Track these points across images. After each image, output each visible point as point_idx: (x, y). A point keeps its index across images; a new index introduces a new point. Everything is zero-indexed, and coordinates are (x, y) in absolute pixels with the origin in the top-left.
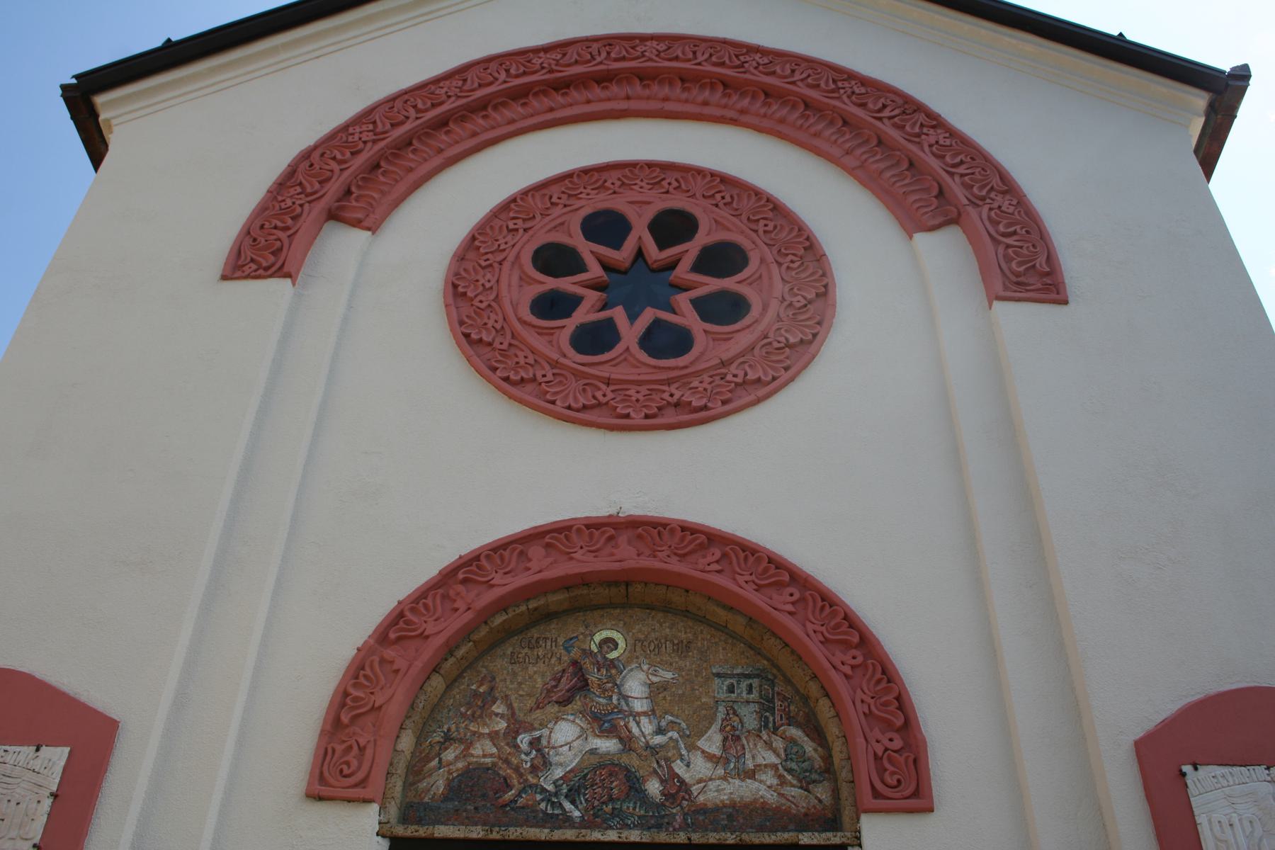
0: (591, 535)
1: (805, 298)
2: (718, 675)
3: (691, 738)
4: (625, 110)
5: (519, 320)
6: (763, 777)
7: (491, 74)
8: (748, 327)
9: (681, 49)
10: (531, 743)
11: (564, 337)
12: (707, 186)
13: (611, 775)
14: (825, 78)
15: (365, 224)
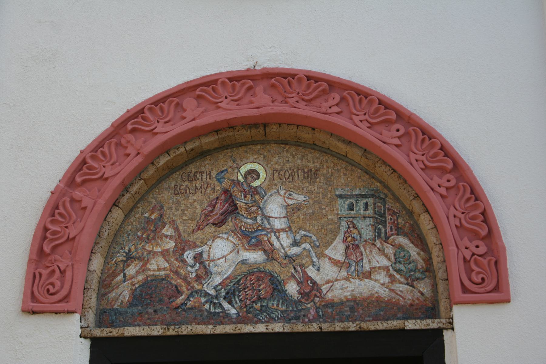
0: (234, 87)
2: (340, 196)
6: (378, 277)
10: (195, 258)
13: (258, 280)
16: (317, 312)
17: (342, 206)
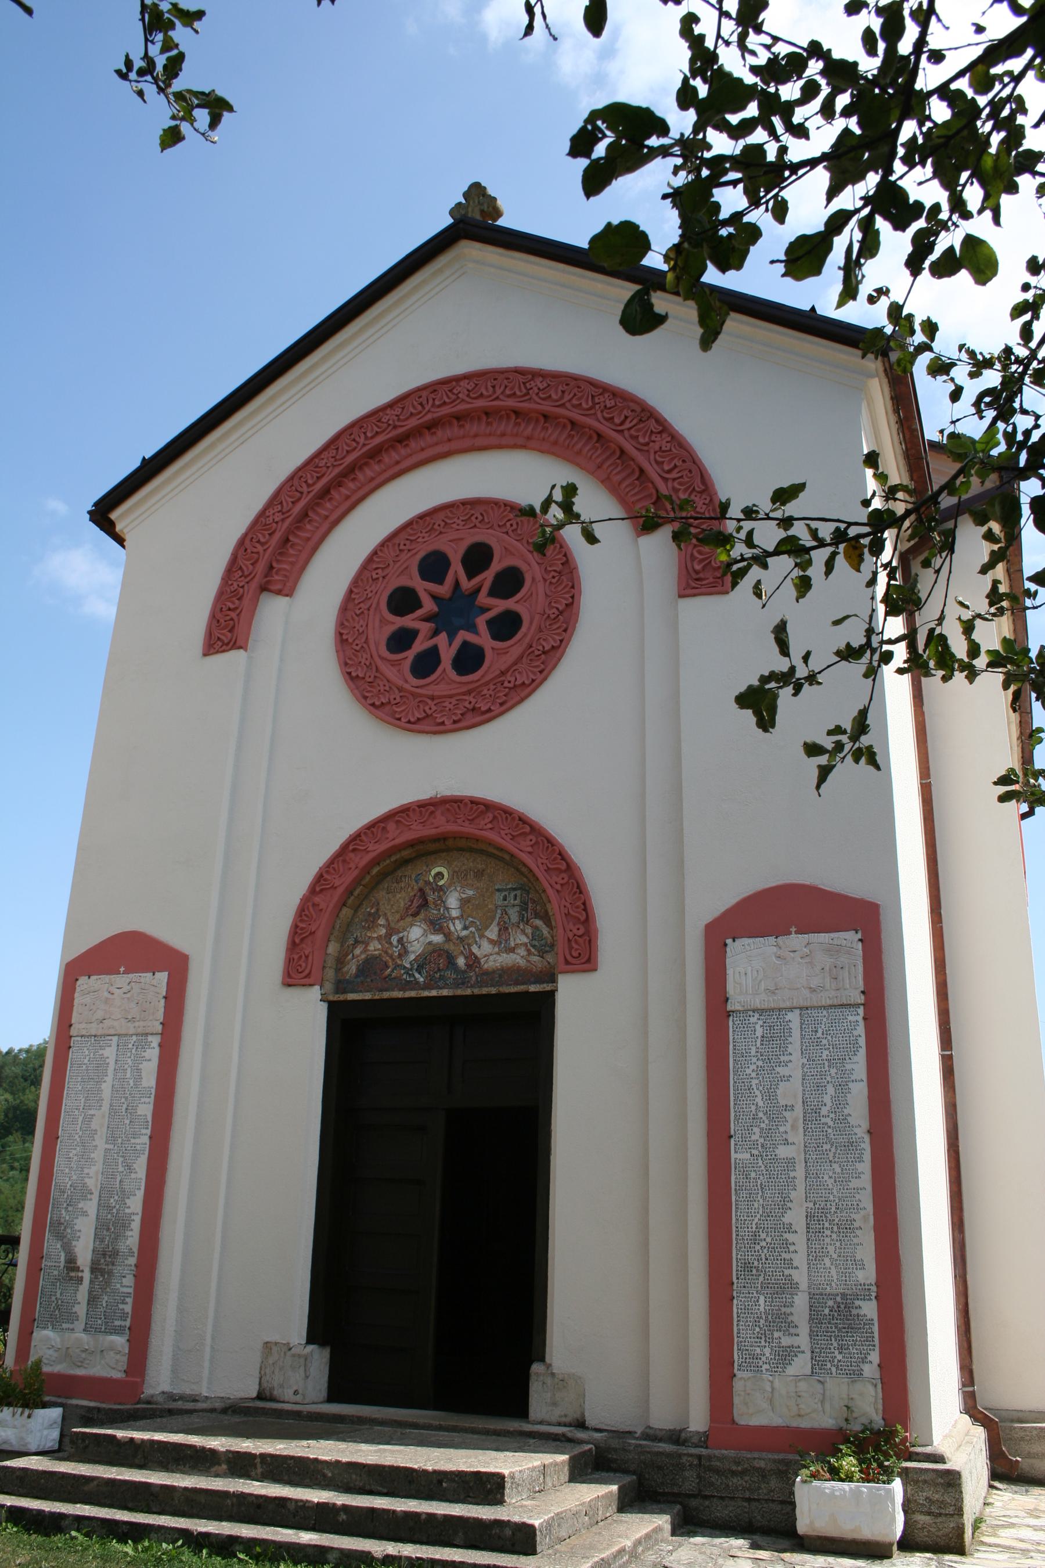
2: (498, 890)
3: (481, 932)
5: (380, 656)
6: (519, 951)
8: (519, 641)
13: (439, 956)
14: (585, 397)
15: (284, 592)
16: (477, 979)
17: (498, 898)
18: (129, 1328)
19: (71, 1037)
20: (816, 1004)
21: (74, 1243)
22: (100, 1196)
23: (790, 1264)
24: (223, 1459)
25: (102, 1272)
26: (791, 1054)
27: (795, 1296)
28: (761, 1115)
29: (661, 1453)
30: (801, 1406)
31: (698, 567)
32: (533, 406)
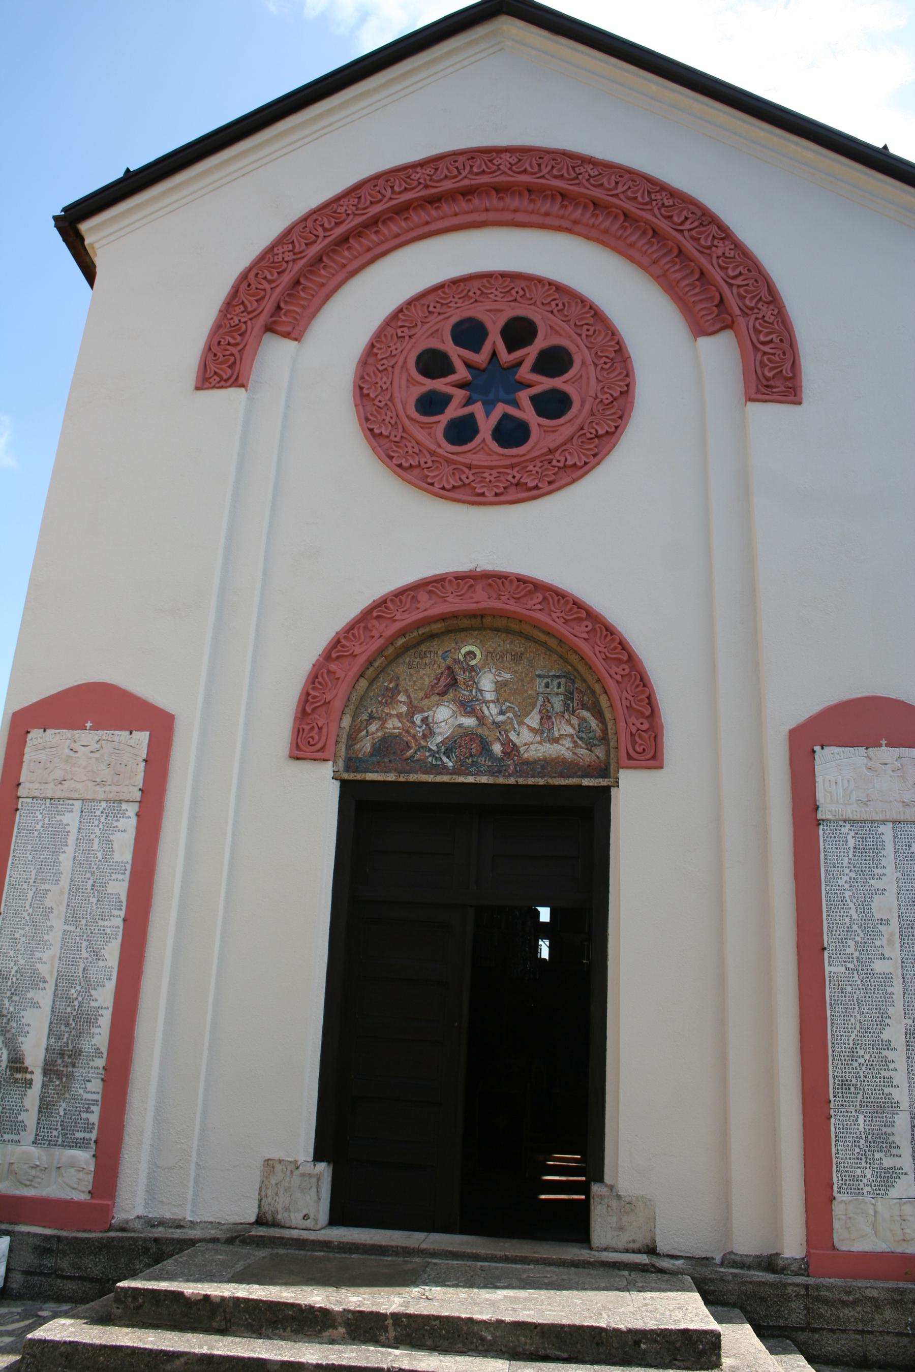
0: (458, 584)
1: (612, 395)
2: (539, 676)
4: (485, 222)
5: (408, 416)
6: (564, 742)
7: (379, 192)
8: (570, 421)
9: (528, 161)
10: (422, 720)
11: (440, 430)
12: (545, 295)
13: (471, 741)
14: (641, 191)
15: (293, 335)
16: (515, 768)
17: (540, 684)
18: (96, 1142)
19: (19, 798)
20: (909, 819)
21: (20, 1039)
22: (56, 986)
23: (889, 1082)
24: (339, 1320)
25: (60, 1076)
26: (884, 867)
27: (895, 1116)
28: (855, 927)
29: (763, 1283)
30: (905, 1231)
31: (770, 375)
32: (582, 190)
